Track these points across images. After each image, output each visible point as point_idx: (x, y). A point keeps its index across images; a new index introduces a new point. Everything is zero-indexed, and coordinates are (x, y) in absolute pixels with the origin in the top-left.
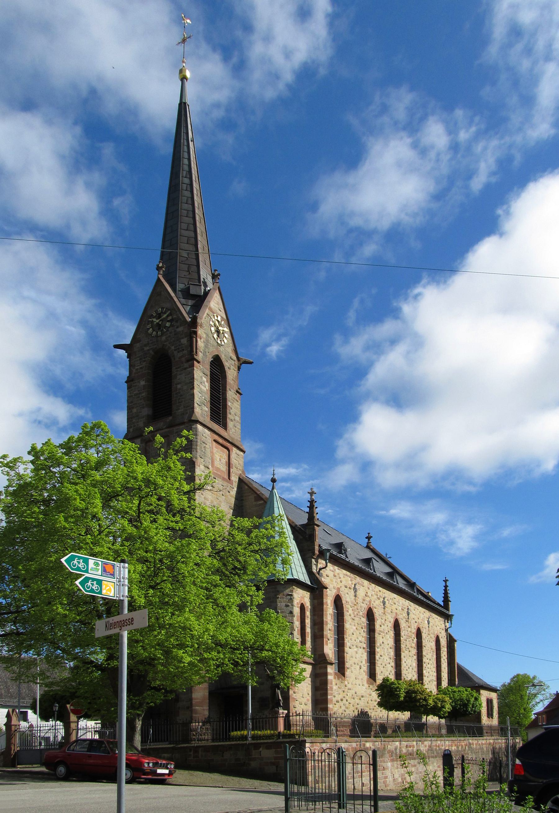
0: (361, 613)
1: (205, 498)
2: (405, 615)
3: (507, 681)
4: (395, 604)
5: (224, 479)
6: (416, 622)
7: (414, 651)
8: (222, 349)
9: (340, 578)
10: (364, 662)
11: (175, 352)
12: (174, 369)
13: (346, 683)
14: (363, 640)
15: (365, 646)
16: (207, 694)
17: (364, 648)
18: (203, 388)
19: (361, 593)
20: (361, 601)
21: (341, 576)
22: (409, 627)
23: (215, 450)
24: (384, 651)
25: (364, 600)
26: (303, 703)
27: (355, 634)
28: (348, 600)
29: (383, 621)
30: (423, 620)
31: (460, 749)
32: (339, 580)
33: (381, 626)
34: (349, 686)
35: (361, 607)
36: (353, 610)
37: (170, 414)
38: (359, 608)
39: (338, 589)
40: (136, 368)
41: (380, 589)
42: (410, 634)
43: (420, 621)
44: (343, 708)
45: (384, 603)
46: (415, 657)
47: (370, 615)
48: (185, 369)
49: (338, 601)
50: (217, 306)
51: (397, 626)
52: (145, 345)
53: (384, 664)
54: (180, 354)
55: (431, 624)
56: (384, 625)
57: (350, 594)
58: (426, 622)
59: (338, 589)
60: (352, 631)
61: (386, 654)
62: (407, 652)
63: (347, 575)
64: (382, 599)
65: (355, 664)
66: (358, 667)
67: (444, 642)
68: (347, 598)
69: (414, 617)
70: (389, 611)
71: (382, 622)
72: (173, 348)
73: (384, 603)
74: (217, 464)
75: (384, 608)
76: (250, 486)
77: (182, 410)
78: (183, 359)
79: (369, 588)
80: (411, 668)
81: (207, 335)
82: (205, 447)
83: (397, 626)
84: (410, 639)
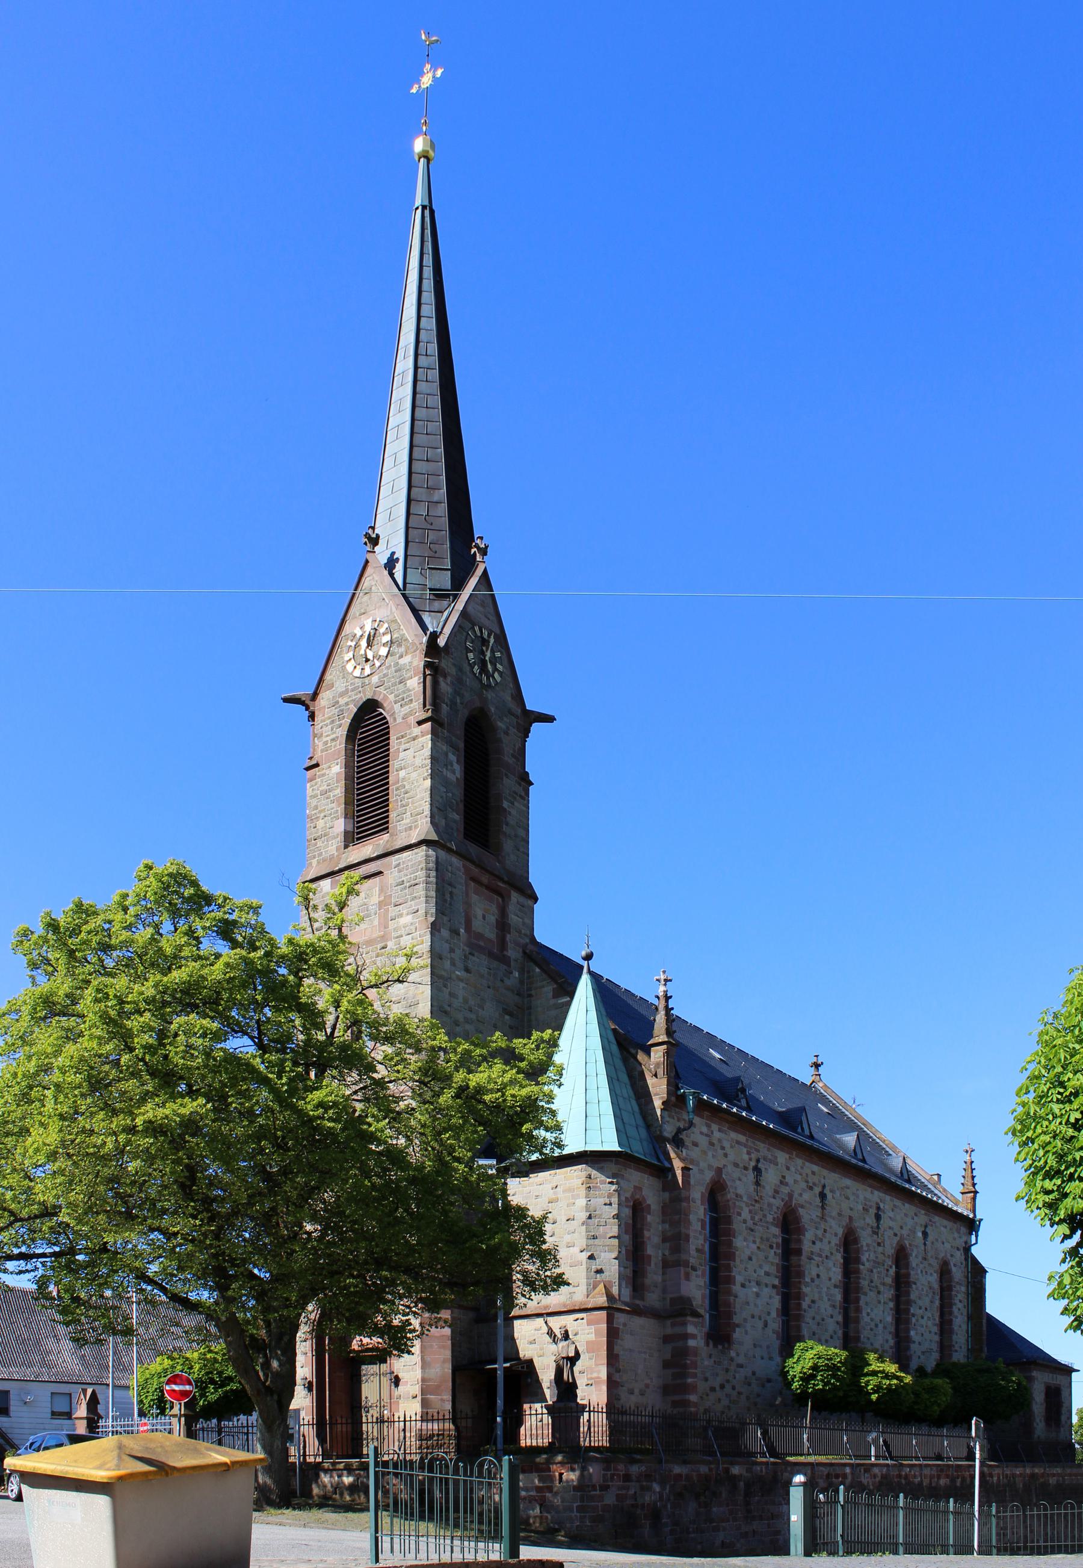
0: (770, 1218)
2: (871, 1220)
4: (847, 1198)
5: (491, 955)
6: (895, 1235)
7: (889, 1293)
8: (489, 695)
9: (723, 1148)
10: (774, 1314)
11: (397, 707)
13: (733, 1354)
14: (773, 1270)
15: (776, 1282)
16: (448, 1369)
17: (774, 1286)
18: (449, 775)
19: (771, 1177)
20: (771, 1193)
21: (726, 1144)
22: (879, 1244)
23: (474, 898)
24: (820, 1292)
25: (776, 1192)
26: (637, 1391)
27: (754, 1258)
28: (740, 1191)
29: (820, 1233)
30: (913, 1231)
31: (958, 1484)
32: (721, 1152)
33: (814, 1243)
34: (741, 1360)
35: (770, 1205)
36: (750, 1212)
38: (765, 1207)
39: (719, 1171)
40: (325, 739)
41: (815, 1168)
42: (881, 1258)
43: (905, 1232)
44: (725, 1402)
45: (823, 1196)
46: (891, 1305)
47: (789, 1224)
49: (716, 1193)
50: (480, 608)
51: (849, 1243)
52: (342, 695)
53: (818, 1318)
54: (406, 709)
55: (930, 1238)
56: (821, 1240)
57: (744, 1179)
58: (920, 1234)
59: (719, 1171)
60: (748, 1253)
61: (825, 1299)
62: (872, 1295)
63: (738, 1142)
64: (817, 1190)
65: (753, 1317)
66: (760, 1324)
67: (958, 1273)
68: (740, 1185)
69: (891, 1224)
70: (834, 1214)
71: (816, 1235)
72: (391, 697)
73: (823, 1196)
74: (477, 925)
75: (823, 1208)
77: (408, 821)
78: (412, 720)
79: (788, 1168)
80: (881, 1326)
81: (460, 669)
82: (451, 893)
83: (849, 1243)
84: (881, 1269)
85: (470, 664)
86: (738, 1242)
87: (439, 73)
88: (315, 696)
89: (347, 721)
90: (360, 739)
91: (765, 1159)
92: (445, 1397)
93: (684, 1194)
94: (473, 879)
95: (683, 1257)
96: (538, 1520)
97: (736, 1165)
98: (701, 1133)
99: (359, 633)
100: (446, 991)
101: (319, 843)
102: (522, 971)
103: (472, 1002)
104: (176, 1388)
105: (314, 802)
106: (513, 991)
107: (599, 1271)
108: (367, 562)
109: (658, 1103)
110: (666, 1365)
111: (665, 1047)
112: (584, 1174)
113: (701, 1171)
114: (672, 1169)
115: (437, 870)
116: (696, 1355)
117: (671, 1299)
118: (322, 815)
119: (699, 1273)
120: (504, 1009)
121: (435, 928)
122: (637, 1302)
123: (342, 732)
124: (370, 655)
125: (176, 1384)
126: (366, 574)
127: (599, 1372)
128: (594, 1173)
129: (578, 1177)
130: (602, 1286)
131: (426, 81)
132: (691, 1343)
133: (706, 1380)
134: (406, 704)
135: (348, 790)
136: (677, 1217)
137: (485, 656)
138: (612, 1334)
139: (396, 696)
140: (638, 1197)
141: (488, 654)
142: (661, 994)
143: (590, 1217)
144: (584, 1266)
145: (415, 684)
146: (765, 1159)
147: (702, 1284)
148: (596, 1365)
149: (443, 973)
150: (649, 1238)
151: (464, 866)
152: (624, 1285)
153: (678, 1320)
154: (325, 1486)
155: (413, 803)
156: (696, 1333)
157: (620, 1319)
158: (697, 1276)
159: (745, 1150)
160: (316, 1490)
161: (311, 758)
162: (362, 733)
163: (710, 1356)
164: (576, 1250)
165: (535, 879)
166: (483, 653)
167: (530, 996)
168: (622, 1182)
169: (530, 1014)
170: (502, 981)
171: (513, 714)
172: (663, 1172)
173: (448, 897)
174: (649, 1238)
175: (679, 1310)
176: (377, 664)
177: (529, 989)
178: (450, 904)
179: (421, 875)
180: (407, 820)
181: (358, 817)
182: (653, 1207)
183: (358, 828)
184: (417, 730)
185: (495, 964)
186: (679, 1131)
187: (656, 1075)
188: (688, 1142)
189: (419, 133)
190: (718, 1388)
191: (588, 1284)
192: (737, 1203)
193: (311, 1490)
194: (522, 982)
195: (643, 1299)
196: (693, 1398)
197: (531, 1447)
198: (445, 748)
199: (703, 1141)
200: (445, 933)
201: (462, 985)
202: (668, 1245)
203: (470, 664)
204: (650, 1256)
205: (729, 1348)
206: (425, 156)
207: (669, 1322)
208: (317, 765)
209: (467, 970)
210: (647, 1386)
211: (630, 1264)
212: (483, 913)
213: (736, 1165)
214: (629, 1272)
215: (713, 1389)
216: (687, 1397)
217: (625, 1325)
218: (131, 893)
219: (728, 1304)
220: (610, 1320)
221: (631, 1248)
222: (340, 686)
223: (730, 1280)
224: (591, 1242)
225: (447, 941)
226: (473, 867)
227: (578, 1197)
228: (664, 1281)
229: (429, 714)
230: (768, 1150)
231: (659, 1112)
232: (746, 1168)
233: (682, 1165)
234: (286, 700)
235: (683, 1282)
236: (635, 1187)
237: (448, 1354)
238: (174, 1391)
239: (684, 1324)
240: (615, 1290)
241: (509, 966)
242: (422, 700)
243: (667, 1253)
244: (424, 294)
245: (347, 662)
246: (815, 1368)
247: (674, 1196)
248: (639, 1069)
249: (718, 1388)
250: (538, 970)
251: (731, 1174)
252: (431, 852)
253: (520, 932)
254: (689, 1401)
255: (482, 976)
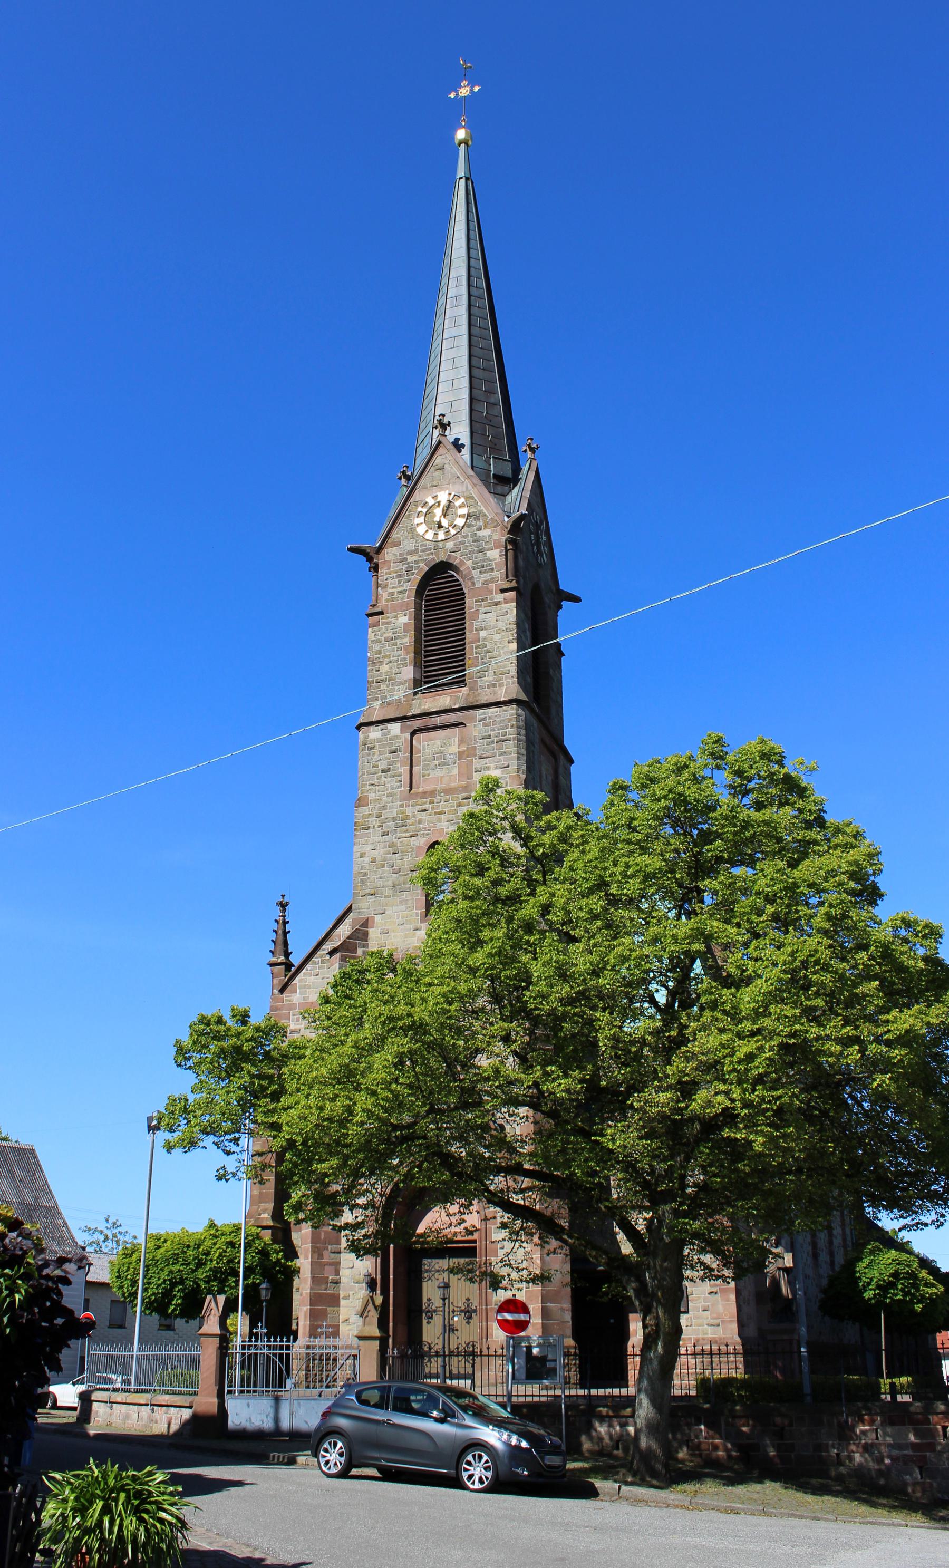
3: (197, 1227)
11: (475, 573)
37: (461, 682)
40: (390, 591)
48: (497, 604)
52: (411, 553)
54: (485, 577)
76: (562, 780)
87: (476, 89)
88: (380, 549)
89: (417, 578)
90: (427, 596)
92: (565, 1306)
96: (919, 1488)
99: (431, 502)
101: (383, 686)
104: (508, 1316)
105: (377, 647)
118: (387, 660)
123: (411, 586)
124: (445, 523)
125: (508, 1312)
126: (438, 453)
131: (464, 92)
134: (486, 571)
135: (417, 641)
139: (473, 563)
145: (495, 555)
154: (601, 1439)
160: (587, 1445)
161: (374, 606)
162: (430, 590)
176: (453, 532)
179: (511, 732)
180: (489, 678)
181: (425, 667)
183: (425, 677)
184: (500, 597)
189: (461, 127)
193: (580, 1445)
206: (465, 142)
208: (381, 613)
218: (697, 754)
222: (408, 545)
229: (514, 584)
234: (351, 550)
238: (507, 1321)
242: (504, 570)
244: (472, 242)
246: (896, 1275)
252: (520, 711)
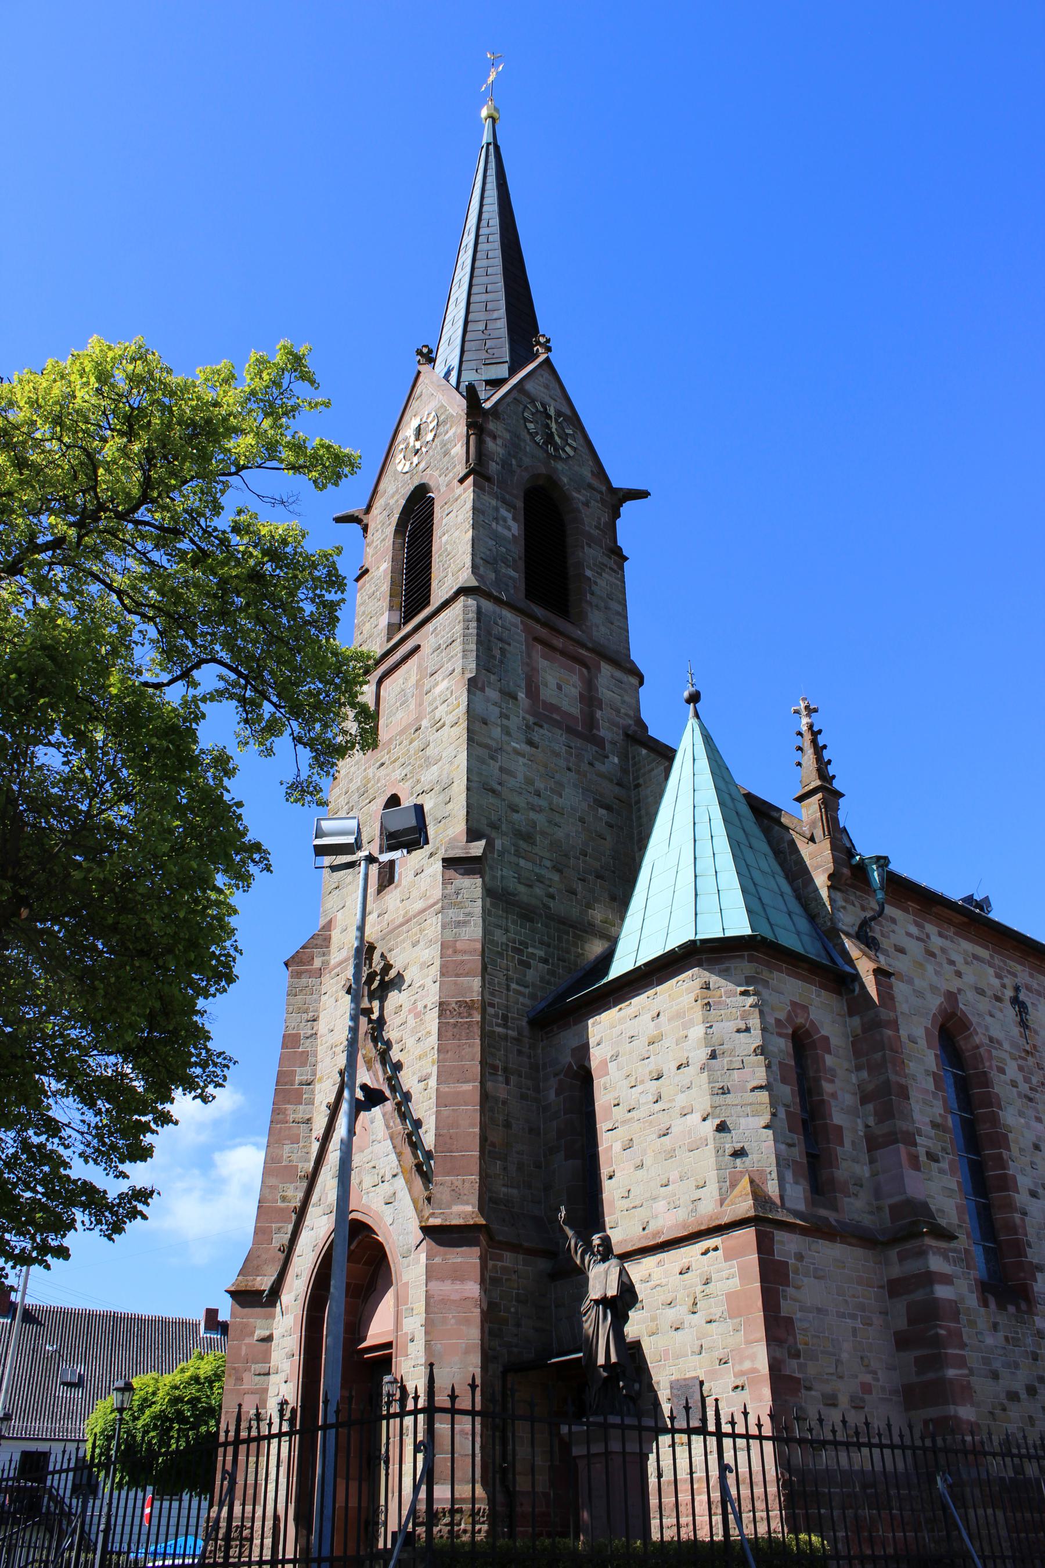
1: (501, 769)
5: (570, 731)
9: (952, 963)
12: (791, 1051)
23: (542, 663)
26: (844, 1400)
28: (997, 1033)
39: (951, 997)
49: (951, 1032)
60: (1030, 1137)
63: (976, 957)
85: (530, 434)
86: (1009, 1117)
91: (1028, 988)
93: (885, 1014)
94: (537, 639)
95: (902, 1125)
97: (981, 992)
98: (909, 934)
100: (494, 766)
102: (624, 757)
103: (540, 784)
106: (611, 781)
107: (739, 1153)
108: (419, 372)
109: (821, 880)
110: (902, 1342)
111: (820, 795)
112: (698, 983)
113: (919, 994)
114: (856, 977)
115: (478, 620)
116: (956, 1315)
117: (892, 1207)
119: (945, 1165)
120: (595, 800)
121: (473, 685)
122: (823, 1212)
127: (753, 1357)
128: (714, 980)
129: (689, 991)
130: (745, 1181)
132: (942, 1292)
133: (995, 1376)
136: (878, 1056)
137: (550, 429)
138: (773, 1277)
140: (800, 1020)
141: (554, 426)
142: (804, 729)
143: (713, 1056)
144: (711, 1146)
146: (1028, 988)
147: (955, 1186)
148: (749, 1342)
149: (489, 742)
150: (834, 1095)
151: (522, 622)
152: (789, 1176)
153: (908, 1246)
155: (454, 562)
156: (954, 1277)
157: (787, 1244)
158: (941, 1171)
159: (991, 971)
163: (995, 1327)
164: (696, 1117)
165: (637, 655)
166: (548, 426)
167: (638, 786)
168: (766, 993)
169: (639, 810)
170: (591, 764)
171: (594, 489)
172: (841, 980)
173: (497, 653)
174: (834, 1095)
175: (908, 1227)
177: (636, 778)
178: (501, 662)
182: (834, 1041)
184: (459, 489)
185: (579, 743)
186: (865, 924)
187: (812, 839)
188: (885, 943)
190: (1023, 1395)
191: (721, 1180)
192: (994, 1052)
194: (625, 771)
195: (835, 1209)
196: (966, 1413)
197: (695, 1542)
198: (494, 502)
199: (915, 948)
200: (493, 694)
201: (521, 760)
202: (870, 1107)
203: (530, 434)
204: (840, 1128)
205: (1031, 1312)
207: (893, 1254)
209: (530, 743)
210: (866, 1388)
211: (797, 1138)
212: (561, 686)
213: (981, 992)
214: (797, 1153)
215: (1013, 1396)
216: (952, 1409)
217: (800, 1257)
219: (1013, 1229)
220: (764, 1246)
221: (796, 1109)
223: (1007, 1183)
224: (720, 1099)
225: (495, 704)
226: (538, 627)
227: (691, 1024)
228: (874, 1174)
230: (1031, 976)
231: (824, 893)
232: (998, 999)
233: (872, 966)
235: (909, 1174)
236: (794, 1004)
237: (473, 1334)
239: (922, 1253)
240: (772, 1188)
241: (604, 748)
243: (871, 1122)
245: (400, 464)
247: (872, 1026)
248: (787, 838)
249: (1023, 1395)
250: (644, 751)
251: (972, 1005)
253: (618, 711)
254: (956, 1418)
255: (557, 755)
